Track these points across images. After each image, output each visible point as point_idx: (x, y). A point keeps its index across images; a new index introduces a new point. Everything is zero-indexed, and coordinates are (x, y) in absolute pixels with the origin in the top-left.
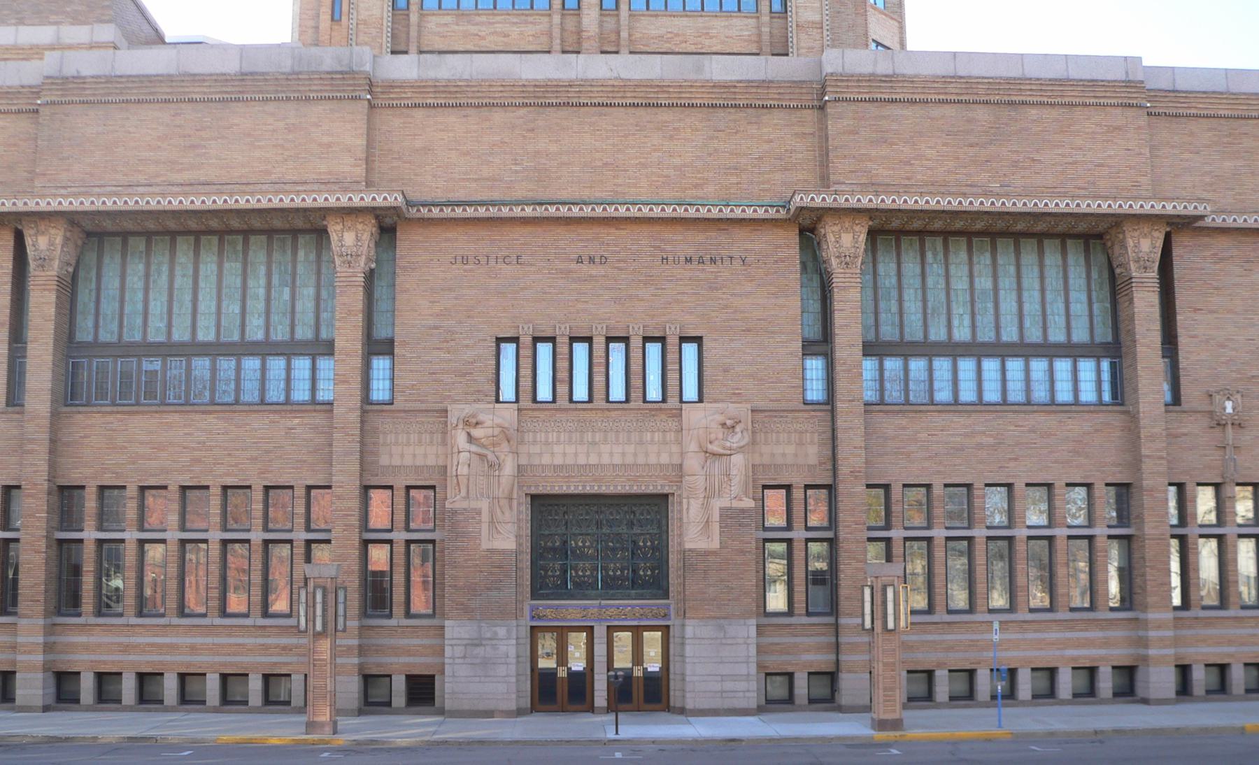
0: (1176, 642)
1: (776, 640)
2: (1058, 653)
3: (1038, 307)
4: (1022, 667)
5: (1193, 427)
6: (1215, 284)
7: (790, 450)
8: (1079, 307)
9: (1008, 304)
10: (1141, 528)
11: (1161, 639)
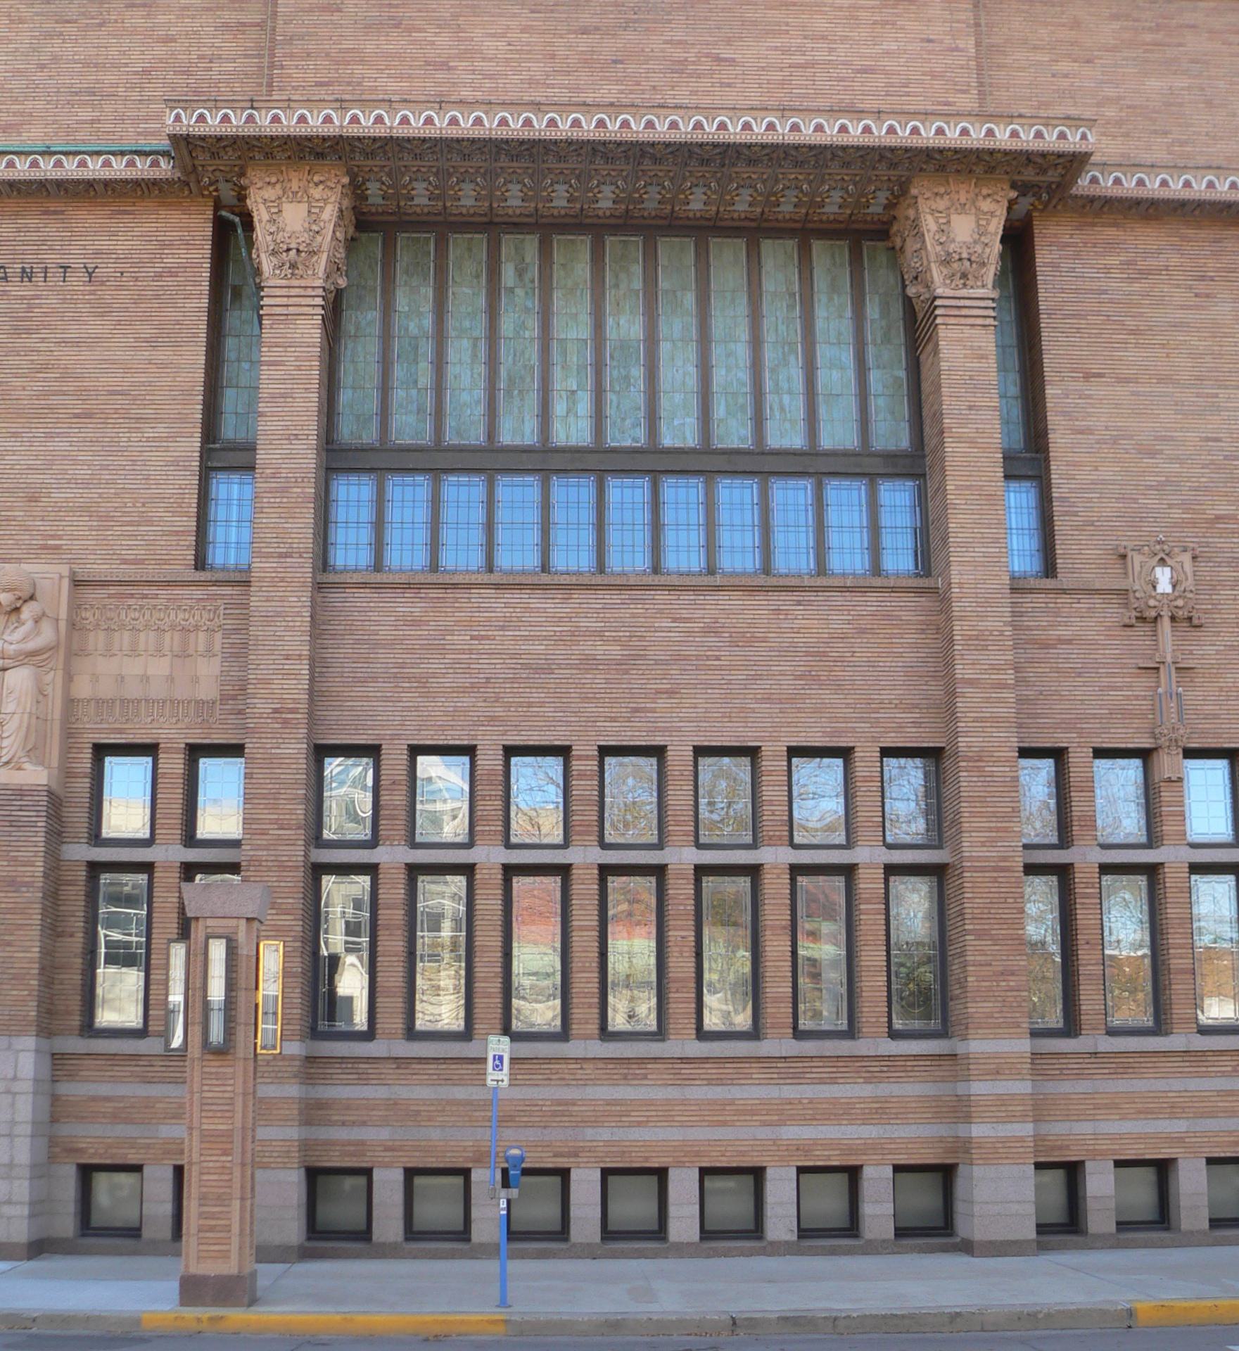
0: (1039, 1109)
1: (104, 1089)
2: (764, 1133)
3: (744, 376)
4: (680, 1165)
5: (1087, 626)
6: (1131, 323)
7: (160, 668)
8: (837, 371)
9: (678, 370)
10: (957, 850)
11: (1002, 1101)
